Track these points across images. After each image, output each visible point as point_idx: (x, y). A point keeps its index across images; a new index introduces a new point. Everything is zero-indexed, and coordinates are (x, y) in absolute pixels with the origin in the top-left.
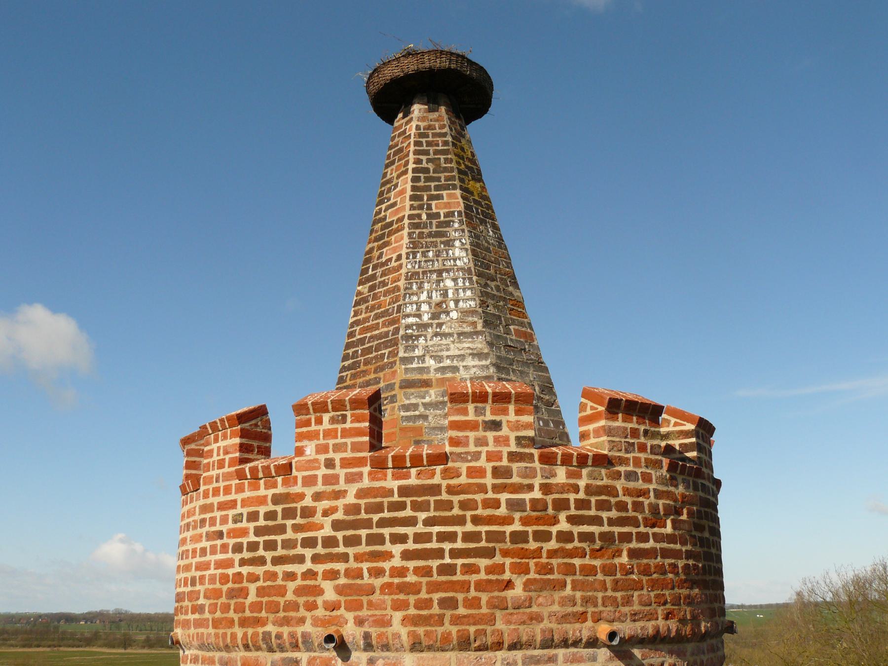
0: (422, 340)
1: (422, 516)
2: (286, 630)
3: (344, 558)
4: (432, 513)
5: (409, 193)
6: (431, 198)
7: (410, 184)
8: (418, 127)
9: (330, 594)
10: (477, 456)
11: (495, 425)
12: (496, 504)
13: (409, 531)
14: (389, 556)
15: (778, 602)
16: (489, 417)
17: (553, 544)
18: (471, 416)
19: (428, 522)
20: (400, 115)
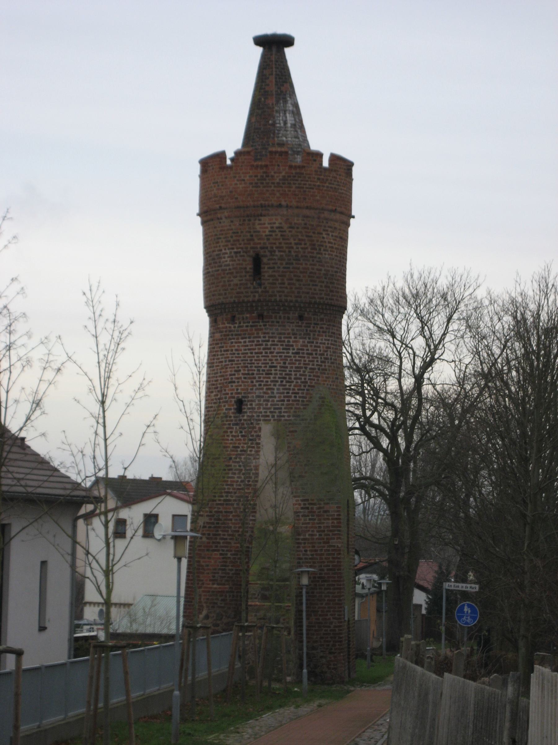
1: (300, 179)
2: (267, 203)
3: (282, 187)
9: (278, 195)
12: (314, 178)
15: (196, 208)
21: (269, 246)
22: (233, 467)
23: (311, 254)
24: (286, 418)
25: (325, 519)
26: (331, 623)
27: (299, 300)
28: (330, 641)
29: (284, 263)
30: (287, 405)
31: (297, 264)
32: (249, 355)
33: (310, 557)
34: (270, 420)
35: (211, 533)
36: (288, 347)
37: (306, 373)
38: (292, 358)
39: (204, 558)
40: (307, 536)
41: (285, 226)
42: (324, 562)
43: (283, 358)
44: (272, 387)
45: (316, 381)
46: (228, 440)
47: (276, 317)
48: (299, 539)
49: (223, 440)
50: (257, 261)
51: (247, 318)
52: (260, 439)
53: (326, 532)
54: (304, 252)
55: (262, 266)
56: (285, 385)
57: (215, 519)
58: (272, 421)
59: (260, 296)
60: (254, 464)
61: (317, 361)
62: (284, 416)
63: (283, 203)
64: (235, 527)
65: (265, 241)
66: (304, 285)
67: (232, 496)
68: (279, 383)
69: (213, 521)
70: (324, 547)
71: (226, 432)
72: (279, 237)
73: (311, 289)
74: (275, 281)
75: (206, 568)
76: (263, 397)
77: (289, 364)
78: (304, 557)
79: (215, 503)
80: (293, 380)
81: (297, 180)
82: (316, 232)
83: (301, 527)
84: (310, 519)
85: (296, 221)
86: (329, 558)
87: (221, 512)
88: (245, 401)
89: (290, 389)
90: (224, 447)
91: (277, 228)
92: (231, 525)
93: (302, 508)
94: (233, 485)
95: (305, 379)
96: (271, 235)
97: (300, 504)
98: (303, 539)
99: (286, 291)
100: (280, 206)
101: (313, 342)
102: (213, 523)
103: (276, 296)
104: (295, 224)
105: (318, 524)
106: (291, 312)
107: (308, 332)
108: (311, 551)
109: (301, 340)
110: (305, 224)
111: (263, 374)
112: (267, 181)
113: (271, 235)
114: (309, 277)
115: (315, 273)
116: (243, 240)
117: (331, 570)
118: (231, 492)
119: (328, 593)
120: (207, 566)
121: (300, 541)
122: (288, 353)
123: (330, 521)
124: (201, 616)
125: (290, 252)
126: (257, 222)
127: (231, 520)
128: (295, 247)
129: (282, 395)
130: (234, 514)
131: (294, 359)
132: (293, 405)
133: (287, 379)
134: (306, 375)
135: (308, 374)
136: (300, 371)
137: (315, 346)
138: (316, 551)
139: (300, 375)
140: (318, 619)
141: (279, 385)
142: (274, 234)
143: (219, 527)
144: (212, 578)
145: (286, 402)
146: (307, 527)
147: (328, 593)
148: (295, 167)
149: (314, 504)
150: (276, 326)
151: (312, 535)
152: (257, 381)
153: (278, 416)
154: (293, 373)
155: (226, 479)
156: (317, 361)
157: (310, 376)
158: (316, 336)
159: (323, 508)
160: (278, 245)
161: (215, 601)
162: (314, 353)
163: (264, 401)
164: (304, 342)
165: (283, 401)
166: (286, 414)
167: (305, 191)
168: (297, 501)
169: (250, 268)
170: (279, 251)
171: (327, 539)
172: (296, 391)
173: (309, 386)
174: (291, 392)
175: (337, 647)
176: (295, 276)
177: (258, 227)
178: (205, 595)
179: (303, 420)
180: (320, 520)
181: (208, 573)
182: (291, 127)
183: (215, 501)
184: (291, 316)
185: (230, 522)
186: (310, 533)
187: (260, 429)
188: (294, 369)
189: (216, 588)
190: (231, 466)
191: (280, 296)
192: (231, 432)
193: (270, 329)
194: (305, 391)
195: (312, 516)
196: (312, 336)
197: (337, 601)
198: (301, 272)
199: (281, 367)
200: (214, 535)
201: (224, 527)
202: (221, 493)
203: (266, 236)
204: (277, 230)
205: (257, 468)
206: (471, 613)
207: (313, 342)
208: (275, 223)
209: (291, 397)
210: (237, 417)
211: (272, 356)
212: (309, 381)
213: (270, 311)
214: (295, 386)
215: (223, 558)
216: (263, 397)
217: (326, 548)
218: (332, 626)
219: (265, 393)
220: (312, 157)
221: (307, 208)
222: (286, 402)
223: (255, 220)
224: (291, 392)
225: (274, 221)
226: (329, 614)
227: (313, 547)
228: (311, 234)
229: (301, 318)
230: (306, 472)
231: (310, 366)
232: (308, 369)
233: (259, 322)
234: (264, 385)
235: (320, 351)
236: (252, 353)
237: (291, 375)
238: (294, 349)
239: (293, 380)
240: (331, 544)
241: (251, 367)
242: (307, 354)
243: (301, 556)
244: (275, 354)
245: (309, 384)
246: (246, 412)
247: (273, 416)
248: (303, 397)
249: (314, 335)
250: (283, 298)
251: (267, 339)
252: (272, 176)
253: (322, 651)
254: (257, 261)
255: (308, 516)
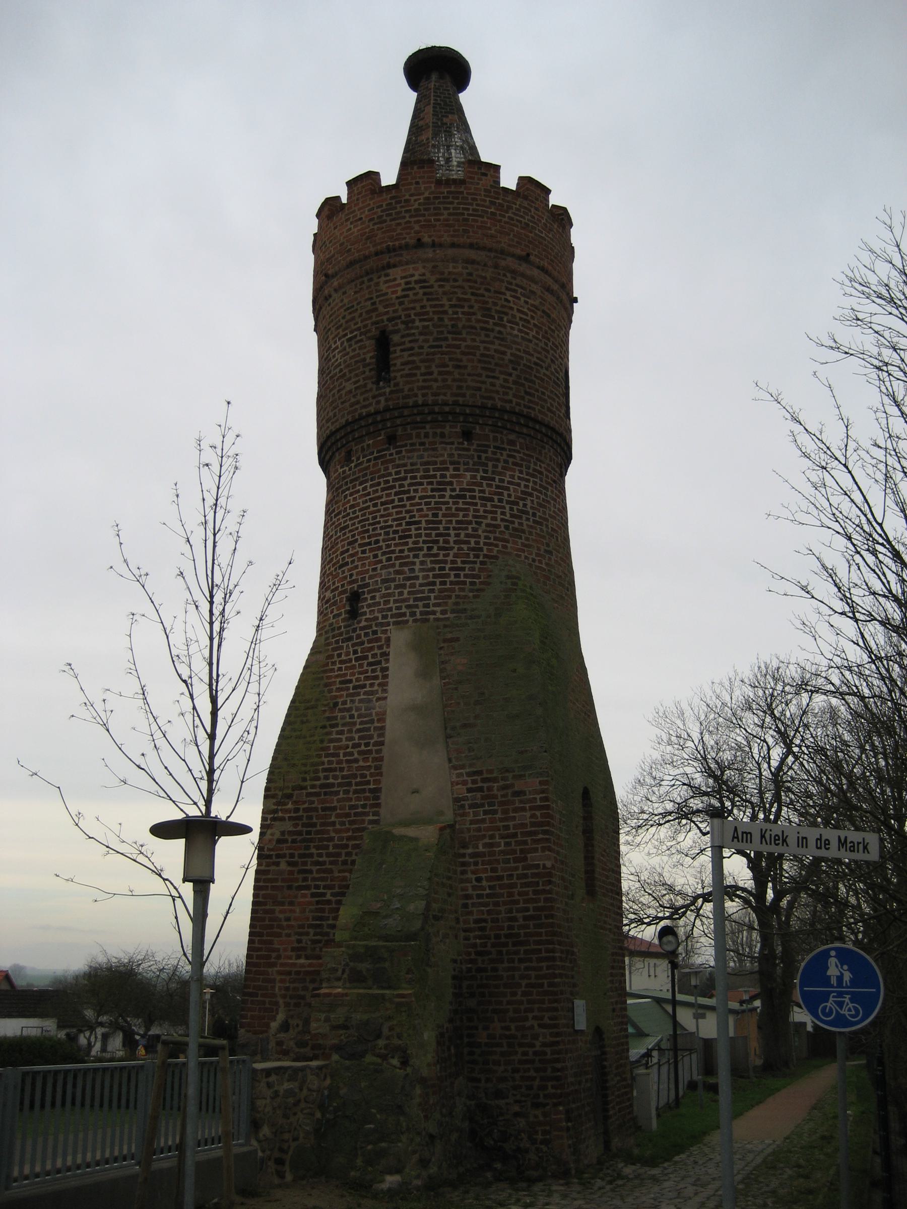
0: (441, 171)
2: (397, 243)
3: (424, 215)
4: (460, 201)
5: (432, 112)
6: (443, 116)
7: (432, 109)
8: (435, 85)
9: (417, 228)
10: (478, 184)
11: (486, 175)
13: (451, 206)
14: (442, 214)
16: (483, 171)
17: (506, 219)
18: (476, 170)
19: (458, 203)
20: (424, 80)
21: (403, 314)
22: (339, 721)
23: (482, 325)
24: (439, 615)
25: (516, 810)
26: (535, 1037)
27: (461, 400)
28: (534, 1079)
29: (431, 338)
30: (440, 591)
31: (453, 339)
32: (372, 509)
33: (488, 891)
34: (407, 621)
35: (296, 853)
36: (440, 489)
37: (480, 532)
38: (451, 505)
39: (282, 904)
40: (481, 849)
41: (432, 280)
42: (517, 902)
43: (433, 505)
44: (411, 559)
45: (500, 548)
46: (332, 670)
47: (418, 436)
48: (464, 855)
49: (325, 672)
50: (383, 343)
51: (368, 445)
52: (387, 661)
53: (519, 838)
54: (469, 320)
55: (392, 349)
56: (437, 555)
57: (304, 825)
58: (410, 623)
59: (387, 400)
60: (378, 709)
61: (503, 513)
62: (434, 613)
63: (426, 239)
64: (341, 839)
65: (397, 307)
66: (469, 375)
67: (335, 777)
68: (425, 551)
69: (299, 828)
70: (516, 868)
71: (331, 656)
72: (420, 296)
73: (484, 382)
74: (414, 372)
75: (285, 923)
76: (394, 580)
77: (444, 515)
78: (475, 893)
79: (304, 791)
80: (452, 544)
81: (452, 203)
82: (492, 289)
83: (469, 830)
84: (485, 812)
85: (451, 270)
86: (527, 893)
87: (316, 809)
88: (364, 592)
89: (445, 562)
90: (326, 685)
91: (416, 282)
92: (333, 834)
93: (469, 790)
94: (338, 755)
95: (477, 543)
96: (406, 296)
97: (464, 783)
98: (473, 855)
99: (435, 385)
100: (420, 244)
101: (493, 479)
102: (300, 833)
103: (416, 396)
104: (450, 273)
105: (501, 820)
106: (448, 425)
107: (483, 460)
108: (489, 879)
109: (468, 474)
110: (470, 274)
111: (394, 539)
112: (398, 209)
113: (406, 296)
114: (480, 361)
115: (493, 357)
116: (361, 315)
117: (532, 918)
118: (335, 770)
119: (527, 969)
120: (288, 919)
121: (467, 859)
122: (443, 496)
123: (528, 814)
124: (274, 1025)
125: (441, 319)
126: (383, 279)
127: (333, 824)
128: (450, 312)
129: (431, 574)
130: (338, 811)
131: (454, 507)
132: (453, 590)
133: (441, 544)
134: (479, 537)
135: (483, 535)
136: (467, 529)
137: (498, 487)
138: (500, 878)
139: (467, 535)
140: (508, 1028)
141: (425, 556)
142: (410, 293)
143: (311, 840)
144: (296, 945)
145: (438, 587)
146: (479, 830)
147: (527, 969)
148: (449, 182)
149: (495, 780)
150: (419, 450)
151: (491, 845)
152: (384, 554)
153: (422, 613)
154: (452, 532)
155: (325, 744)
156: (503, 513)
157: (486, 538)
158: (500, 469)
159: (512, 785)
160: (418, 310)
161: (302, 993)
162: (496, 498)
163: (396, 587)
164: (474, 477)
165: (434, 584)
166: (438, 609)
167: (467, 220)
168: (459, 775)
169: (371, 358)
170: (421, 320)
171: (522, 851)
172: (460, 565)
173: (485, 556)
174: (448, 566)
175: (551, 1090)
176: (451, 359)
177: (383, 287)
178: (282, 981)
179: (471, 618)
180: (505, 812)
181: (289, 935)
182: (458, 166)
183: (305, 788)
184: (447, 430)
185: (331, 828)
186: (487, 840)
187: (388, 640)
188: (454, 525)
189: (302, 966)
190: (336, 718)
191: (424, 395)
192: (339, 655)
193: (409, 458)
194: (478, 566)
195: (490, 805)
196: (490, 468)
197: (546, 987)
198: (463, 353)
199: (427, 522)
200: (301, 856)
201: (321, 840)
202: (316, 771)
203: (398, 298)
204: (417, 286)
205: (382, 718)
206: (854, 983)
207: (493, 479)
208: (413, 276)
209: (448, 576)
210: (349, 626)
211: (412, 505)
212: (485, 548)
213: (409, 426)
214: (456, 556)
215: (318, 903)
216: (394, 580)
217: (520, 872)
218: (538, 1044)
219: (398, 572)
220: (480, 168)
221: (471, 246)
222: (438, 587)
223: (379, 277)
224: (448, 566)
225: (411, 272)
226: (530, 1015)
227: (494, 870)
228: (481, 291)
229: (467, 435)
230: (476, 717)
231: (489, 521)
232: (483, 525)
233: (388, 449)
234: (397, 558)
235: (509, 496)
236: (375, 505)
237: (449, 535)
238: (453, 490)
239: (452, 544)
240: (530, 862)
241: (374, 530)
242: (481, 498)
243: (470, 892)
244: (417, 500)
245: (485, 552)
246: (365, 613)
247: (413, 614)
248: (473, 576)
249: (495, 466)
250: (430, 399)
251: (403, 475)
252: (407, 201)
253: (516, 1102)
254: (383, 343)
255: (483, 805)
